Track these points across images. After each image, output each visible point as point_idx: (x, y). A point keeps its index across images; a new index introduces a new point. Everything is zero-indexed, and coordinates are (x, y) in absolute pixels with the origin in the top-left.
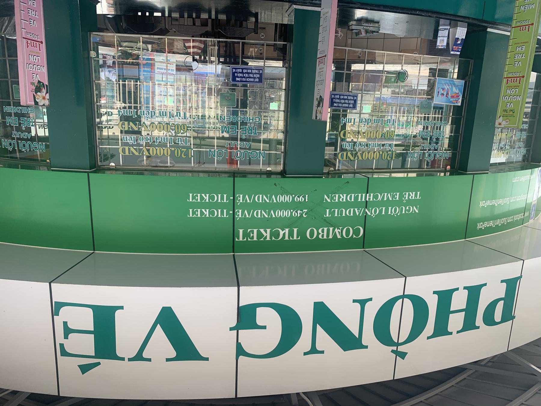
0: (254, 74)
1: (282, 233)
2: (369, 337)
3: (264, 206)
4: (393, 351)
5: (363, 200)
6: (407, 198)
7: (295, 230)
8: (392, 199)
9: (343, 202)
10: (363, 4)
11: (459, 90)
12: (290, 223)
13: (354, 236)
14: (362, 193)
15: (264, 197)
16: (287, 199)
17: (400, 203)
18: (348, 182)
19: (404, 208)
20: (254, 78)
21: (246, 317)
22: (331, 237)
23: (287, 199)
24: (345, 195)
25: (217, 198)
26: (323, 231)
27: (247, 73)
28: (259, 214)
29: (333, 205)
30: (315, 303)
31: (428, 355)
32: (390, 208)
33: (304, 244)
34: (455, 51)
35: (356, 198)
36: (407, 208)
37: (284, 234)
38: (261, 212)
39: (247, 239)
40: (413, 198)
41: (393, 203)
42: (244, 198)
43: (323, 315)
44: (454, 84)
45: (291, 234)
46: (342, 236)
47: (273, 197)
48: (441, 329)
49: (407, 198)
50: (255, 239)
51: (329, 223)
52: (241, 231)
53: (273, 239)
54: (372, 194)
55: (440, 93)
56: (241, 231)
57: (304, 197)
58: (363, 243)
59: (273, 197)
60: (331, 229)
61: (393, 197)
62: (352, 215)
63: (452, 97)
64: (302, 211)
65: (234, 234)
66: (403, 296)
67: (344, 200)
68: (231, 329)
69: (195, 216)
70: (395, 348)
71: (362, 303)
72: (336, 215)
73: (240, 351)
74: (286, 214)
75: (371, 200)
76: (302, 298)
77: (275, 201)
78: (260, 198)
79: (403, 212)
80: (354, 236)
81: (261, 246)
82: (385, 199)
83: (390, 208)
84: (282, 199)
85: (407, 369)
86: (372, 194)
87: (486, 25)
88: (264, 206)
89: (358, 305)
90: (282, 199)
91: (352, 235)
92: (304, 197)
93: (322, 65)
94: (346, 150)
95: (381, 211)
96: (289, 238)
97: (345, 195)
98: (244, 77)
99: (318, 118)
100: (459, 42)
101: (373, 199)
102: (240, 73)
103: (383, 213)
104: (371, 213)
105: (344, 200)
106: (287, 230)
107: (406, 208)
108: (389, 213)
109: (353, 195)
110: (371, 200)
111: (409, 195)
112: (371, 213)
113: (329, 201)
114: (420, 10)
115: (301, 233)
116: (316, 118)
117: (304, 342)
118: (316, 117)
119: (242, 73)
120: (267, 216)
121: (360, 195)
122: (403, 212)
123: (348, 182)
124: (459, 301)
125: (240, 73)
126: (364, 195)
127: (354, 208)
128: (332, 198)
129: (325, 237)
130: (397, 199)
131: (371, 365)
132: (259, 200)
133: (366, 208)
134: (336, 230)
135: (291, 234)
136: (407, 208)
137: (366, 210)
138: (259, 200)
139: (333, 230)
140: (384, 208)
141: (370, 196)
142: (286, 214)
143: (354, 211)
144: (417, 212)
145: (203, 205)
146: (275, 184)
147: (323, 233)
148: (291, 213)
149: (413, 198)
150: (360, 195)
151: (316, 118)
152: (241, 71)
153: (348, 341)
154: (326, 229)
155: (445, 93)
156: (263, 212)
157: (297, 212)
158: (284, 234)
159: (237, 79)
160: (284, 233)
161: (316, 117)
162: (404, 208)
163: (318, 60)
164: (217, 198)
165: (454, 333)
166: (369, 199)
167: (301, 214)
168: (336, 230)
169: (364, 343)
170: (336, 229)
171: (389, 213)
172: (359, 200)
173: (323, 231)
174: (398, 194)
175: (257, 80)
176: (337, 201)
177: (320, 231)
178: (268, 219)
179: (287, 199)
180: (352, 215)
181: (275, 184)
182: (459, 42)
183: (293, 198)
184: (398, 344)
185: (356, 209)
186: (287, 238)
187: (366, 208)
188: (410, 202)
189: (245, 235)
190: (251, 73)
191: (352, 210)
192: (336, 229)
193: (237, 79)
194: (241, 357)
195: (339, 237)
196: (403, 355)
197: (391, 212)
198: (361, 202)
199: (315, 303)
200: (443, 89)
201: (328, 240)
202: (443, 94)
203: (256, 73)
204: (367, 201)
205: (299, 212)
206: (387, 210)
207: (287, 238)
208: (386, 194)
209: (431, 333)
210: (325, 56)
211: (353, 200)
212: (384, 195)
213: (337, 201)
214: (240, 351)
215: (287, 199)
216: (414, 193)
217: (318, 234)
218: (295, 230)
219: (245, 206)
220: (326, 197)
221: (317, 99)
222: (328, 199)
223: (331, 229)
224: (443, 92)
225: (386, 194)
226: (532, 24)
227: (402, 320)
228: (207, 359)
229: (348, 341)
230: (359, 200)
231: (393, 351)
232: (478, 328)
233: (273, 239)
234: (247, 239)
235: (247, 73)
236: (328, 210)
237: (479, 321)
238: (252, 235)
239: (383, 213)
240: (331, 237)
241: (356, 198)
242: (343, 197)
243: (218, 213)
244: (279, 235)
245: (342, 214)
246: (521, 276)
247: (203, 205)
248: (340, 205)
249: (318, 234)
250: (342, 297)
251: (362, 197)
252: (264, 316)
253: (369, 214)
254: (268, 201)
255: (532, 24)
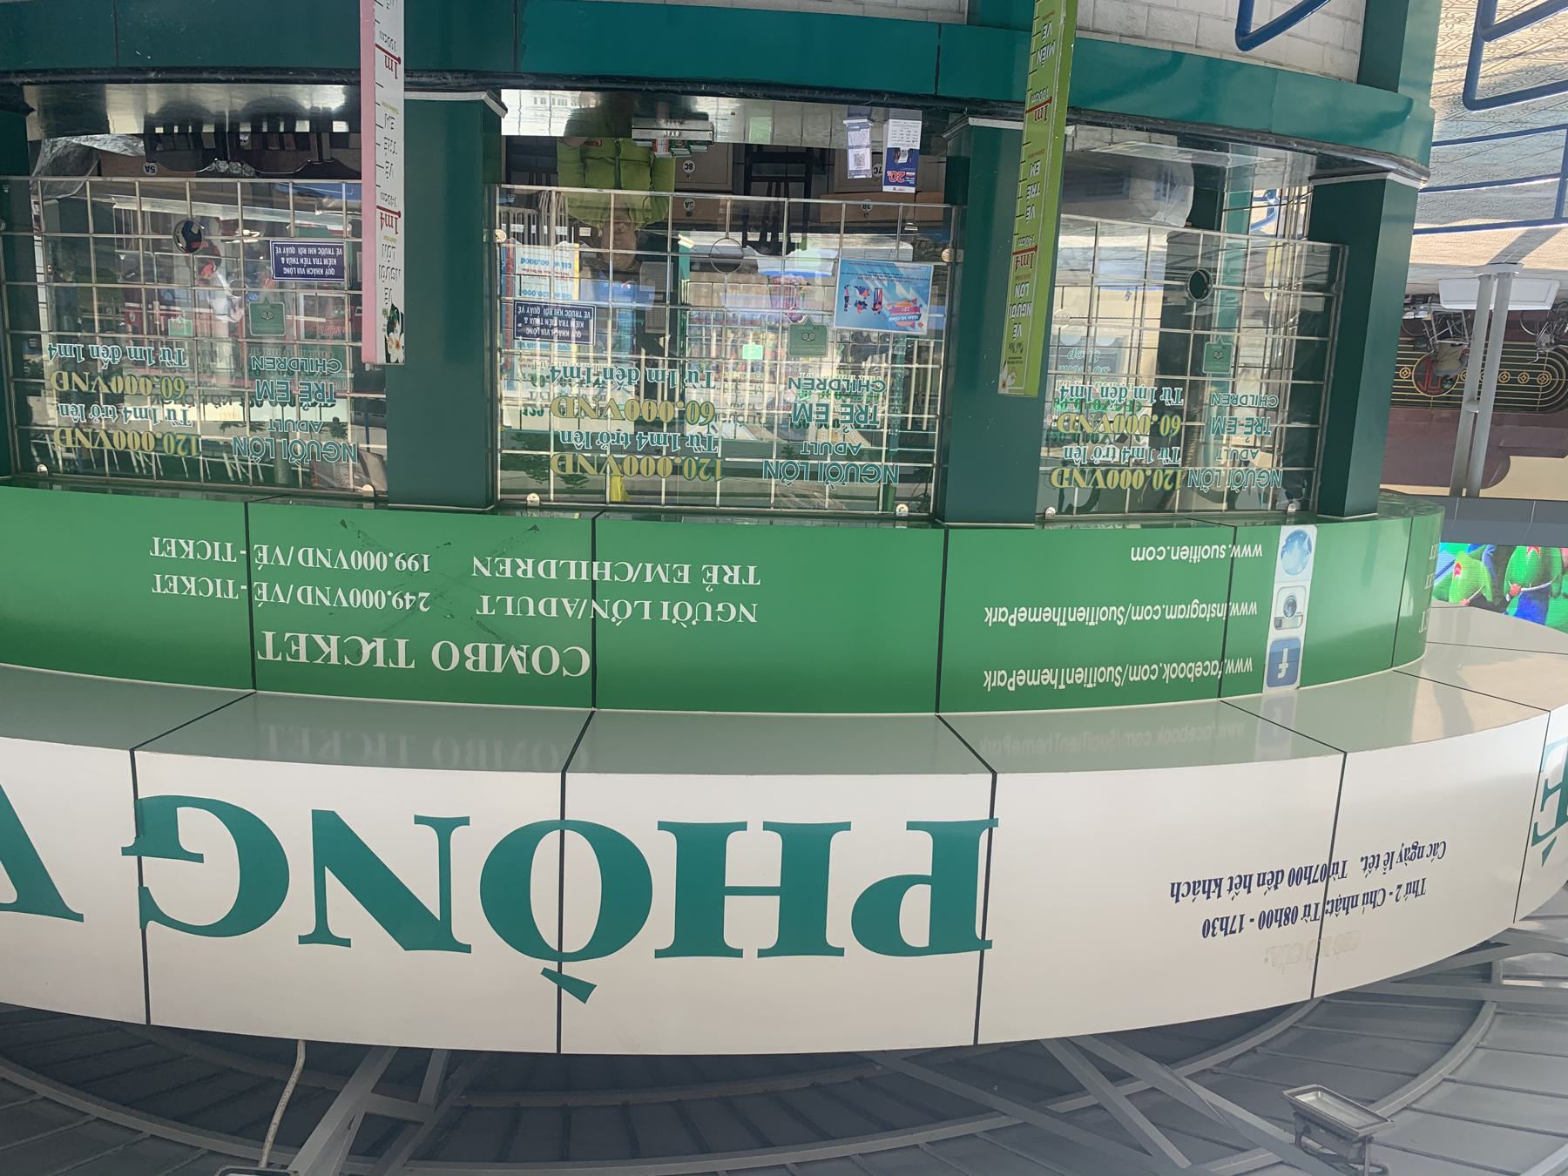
0: (323, 257)
1: (367, 649)
2: (469, 918)
3: (317, 577)
4: (546, 972)
5: (584, 577)
6: (715, 581)
7: (402, 643)
8: (670, 579)
9: (541, 586)
10: (330, 72)
11: (917, 290)
12: (386, 625)
13: (565, 673)
14: (579, 559)
15: (319, 554)
16: (376, 561)
17: (694, 592)
18: (535, 528)
19: (709, 607)
20: (325, 267)
21: (155, 828)
22: (498, 668)
23: (376, 561)
24: (530, 562)
25: (213, 550)
26: (475, 651)
27: (307, 255)
28: (310, 595)
29: (497, 586)
30: (316, 815)
31: (652, 1005)
32: (666, 604)
33: (425, 682)
34: (897, 184)
35: (563, 571)
36: (720, 608)
37: (374, 651)
38: (313, 592)
39: (284, 657)
40: (736, 581)
41: (675, 592)
42: (271, 553)
43: (337, 845)
44: (899, 277)
45: (391, 652)
46: (530, 667)
47: (341, 554)
48: (700, 932)
49: (715, 581)
50: (303, 658)
51: (491, 631)
52: (269, 635)
53: (347, 661)
54: (608, 565)
55: (852, 301)
56: (269, 635)
57: (419, 559)
58: (594, 690)
59: (341, 554)
60: (498, 648)
61: (673, 574)
62: (554, 614)
63: (895, 310)
64: (416, 594)
65: (254, 644)
66: (563, 825)
67: (530, 575)
68: (126, 851)
69: (166, 591)
70: (553, 966)
71: (445, 828)
72: (510, 612)
73: (149, 910)
74: (374, 599)
75: (607, 578)
76: (287, 793)
77: (346, 566)
78: (311, 557)
79: (709, 618)
80: (565, 673)
81: (314, 677)
82: (649, 579)
83: (666, 604)
84: (362, 560)
85: (594, 1031)
86: (608, 565)
87: (17, 81)
88: (317, 577)
89: (430, 834)
90: (362, 560)
91: (560, 671)
92: (419, 559)
93: (1023, 270)
94: (571, 447)
95: (639, 611)
96: (386, 662)
97: (530, 562)
98: (301, 266)
99: (393, 360)
100: (903, 160)
101: (612, 577)
102: (291, 255)
103: (647, 617)
104: (612, 612)
105: (530, 575)
106: (380, 642)
107: (714, 607)
108: (665, 617)
109: (553, 563)
110: (607, 578)
111: (722, 573)
112: (611, 614)
113: (487, 573)
114: (707, 82)
115: (418, 653)
116: (388, 360)
117: (297, 909)
118: (388, 356)
119: (296, 255)
120: (327, 603)
121: (573, 563)
122: (709, 618)
123: (535, 528)
124: (754, 860)
125: (291, 255)
126: (584, 564)
127: (559, 596)
128: (494, 568)
129: (483, 668)
130: (686, 580)
131: (479, 1000)
132: (306, 561)
133: (594, 597)
134: (512, 651)
135: (391, 652)
136: (720, 608)
137: (594, 605)
138: (306, 561)
139: (505, 652)
140: (647, 604)
141: (602, 567)
142: (374, 599)
143: (560, 605)
144: (752, 620)
145: (181, 566)
146: (343, 523)
147: (477, 657)
148: (389, 599)
149: (736, 581)
150: (573, 563)
151: (388, 360)
152: (293, 251)
153: (418, 927)
154: (483, 647)
155: (870, 301)
156: (318, 592)
157: (402, 596)
158: (374, 651)
159: (287, 271)
160: (372, 649)
161: (388, 356)
162: (709, 607)
163: (1014, 258)
164: (213, 550)
165: (750, 953)
166: (601, 575)
167: (415, 604)
168: (512, 651)
169: (459, 934)
170: (513, 649)
171: (665, 617)
172: (573, 577)
173: (475, 651)
174: (686, 567)
175: (332, 272)
176: (508, 574)
177: (468, 650)
178: (331, 612)
179: (375, 561)
180: (554, 614)
181: (343, 523)
182: (903, 160)
183: (391, 561)
184: (560, 956)
185: (565, 601)
186: (380, 663)
187: (594, 597)
188: (725, 592)
189: (280, 646)
190: (317, 256)
191: (554, 601)
192: (513, 649)
193: (287, 271)
194: (151, 924)
195: (521, 670)
196: (582, 990)
197: (671, 615)
198: (578, 581)
199: (316, 815)
200: (861, 290)
201: (490, 676)
202: (861, 305)
203: (328, 256)
204: (594, 582)
205: (408, 597)
206: (656, 610)
207: (380, 663)
208: (649, 566)
209: (668, 941)
210: (1035, 249)
211: (553, 576)
212: (644, 568)
213: (508, 574)
214: (149, 910)
215: (375, 561)
216: (736, 568)
217: (463, 658)
218: (402, 643)
219: (275, 574)
220: (476, 562)
221: (385, 312)
222: (483, 570)
223: (498, 648)
224: (861, 298)
225: (649, 566)
226: (1050, 101)
227: (568, 893)
228: (79, 918)
229: (418, 927)
230: (573, 577)
231: (546, 972)
232: (839, 952)
233: (347, 661)
234: (284, 657)
235: (307, 255)
236: (485, 598)
237: (838, 927)
238: (294, 648)
239: (647, 617)
240: (498, 668)
241: (563, 571)
242: (526, 568)
243: (215, 588)
244: (359, 653)
245: (525, 610)
246: (991, 823)
247: (181, 566)
248: (518, 586)
249: (463, 658)
250: (388, 803)
251: (579, 570)
252: (195, 828)
253: (605, 616)
254: (328, 565)
255: (1050, 101)
